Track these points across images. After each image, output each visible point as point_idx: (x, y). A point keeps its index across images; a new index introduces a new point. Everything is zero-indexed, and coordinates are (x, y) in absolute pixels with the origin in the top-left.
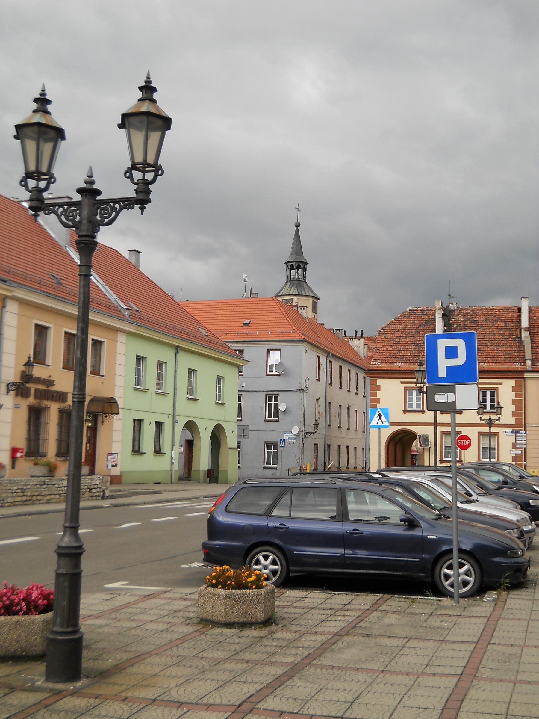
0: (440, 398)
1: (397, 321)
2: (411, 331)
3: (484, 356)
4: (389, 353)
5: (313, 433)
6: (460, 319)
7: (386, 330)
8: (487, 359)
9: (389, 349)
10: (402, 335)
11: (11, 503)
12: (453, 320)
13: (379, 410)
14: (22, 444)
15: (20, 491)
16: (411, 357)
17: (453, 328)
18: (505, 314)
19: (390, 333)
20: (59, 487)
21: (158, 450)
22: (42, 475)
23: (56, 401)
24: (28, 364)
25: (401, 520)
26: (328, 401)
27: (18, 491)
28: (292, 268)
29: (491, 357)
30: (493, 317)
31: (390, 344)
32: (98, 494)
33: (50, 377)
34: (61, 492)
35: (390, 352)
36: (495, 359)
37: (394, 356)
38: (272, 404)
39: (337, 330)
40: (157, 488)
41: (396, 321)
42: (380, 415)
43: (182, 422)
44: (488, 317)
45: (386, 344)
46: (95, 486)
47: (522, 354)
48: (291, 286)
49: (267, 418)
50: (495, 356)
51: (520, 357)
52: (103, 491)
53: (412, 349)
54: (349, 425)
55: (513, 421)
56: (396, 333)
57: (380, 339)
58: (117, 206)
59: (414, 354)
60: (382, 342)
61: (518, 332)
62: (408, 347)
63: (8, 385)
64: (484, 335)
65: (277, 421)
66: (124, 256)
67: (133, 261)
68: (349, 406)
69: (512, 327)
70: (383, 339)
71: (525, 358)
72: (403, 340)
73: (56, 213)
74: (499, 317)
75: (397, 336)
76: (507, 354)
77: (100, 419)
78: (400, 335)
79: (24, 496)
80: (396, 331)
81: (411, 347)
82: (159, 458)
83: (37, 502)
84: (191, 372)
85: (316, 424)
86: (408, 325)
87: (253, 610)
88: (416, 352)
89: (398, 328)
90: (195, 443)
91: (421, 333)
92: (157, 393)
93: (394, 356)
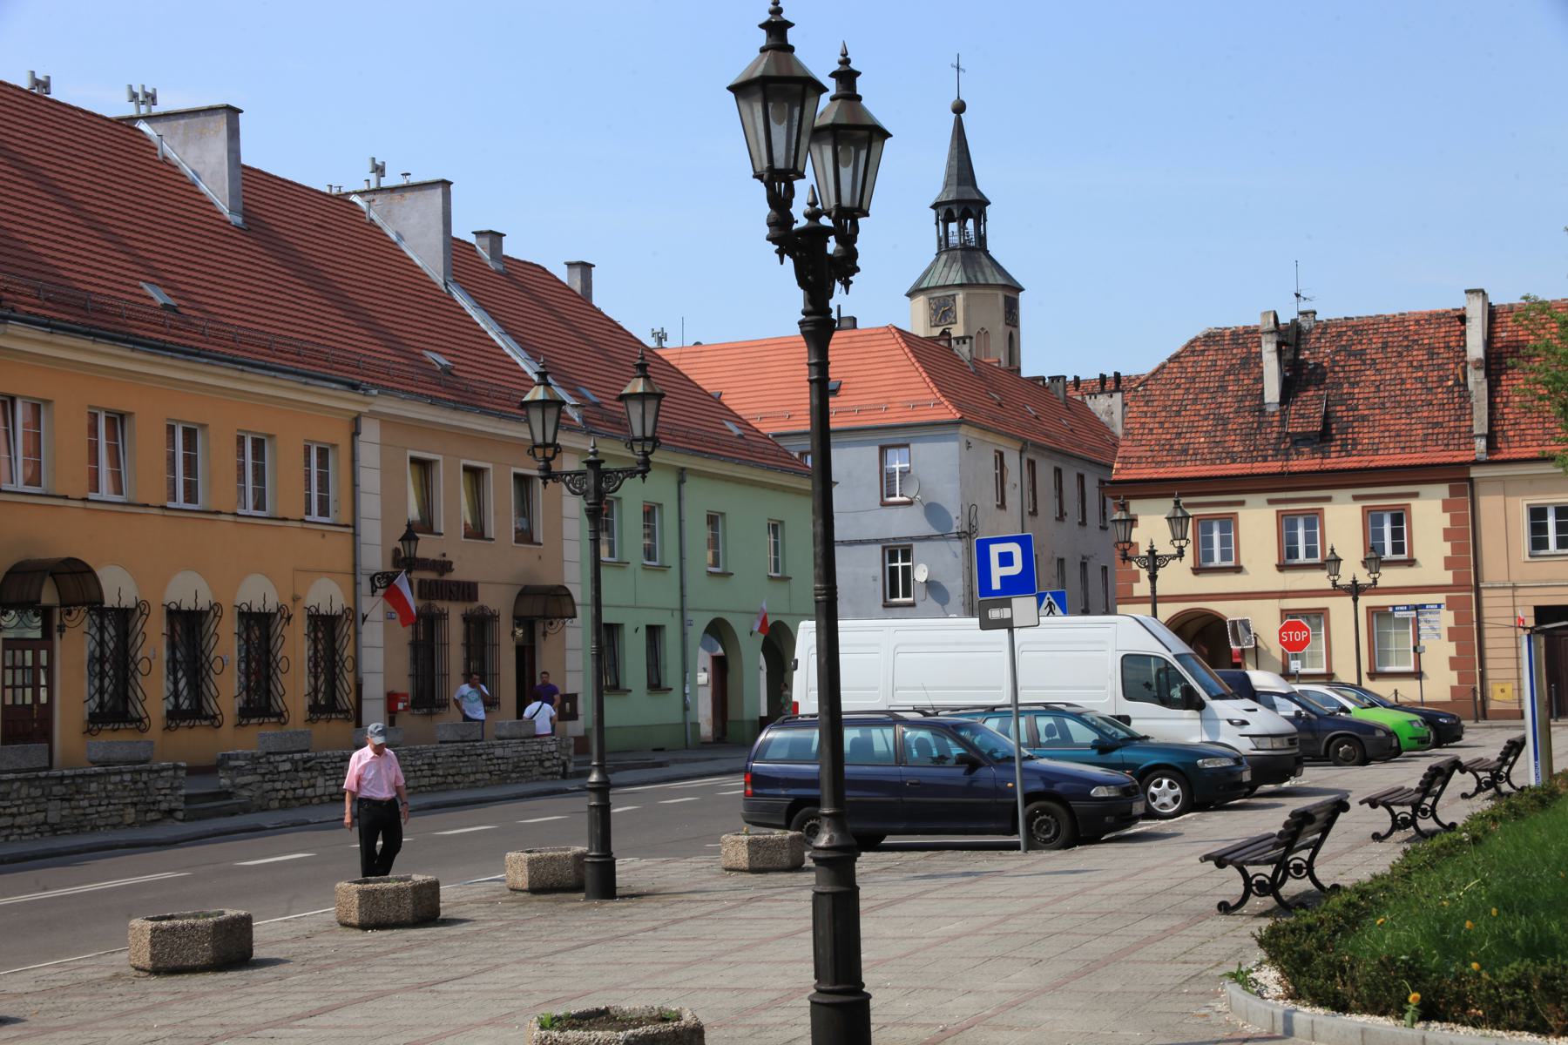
0: (994, 614)
1: (1176, 365)
2: (1207, 385)
3: (1376, 434)
4: (1156, 440)
6: (1322, 350)
7: (1149, 387)
8: (1382, 440)
9: (1155, 431)
10: (1186, 397)
11: (414, 788)
12: (1307, 352)
13: (1048, 595)
14: (404, 685)
15: (426, 767)
16: (1205, 445)
17: (1305, 371)
18: (1432, 331)
19: (1158, 393)
20: (489, 760)
21: (655, 682)
22: (459, 739)
23: (457, 600)
24: (410, 536)
27: (423, 768)
28: (948, 218)
29: (1393, 434)
30: (1401, 339)
31: (1157, 420)
32: (554, 769)
33: (444, 555)
34: (492, 767)
35: (1158, 437)
36: (1403, 439)
37: (1167, 447)
38: (897, 567)
39: (1052, 379)
40: (659, 757)
41: (1171, 365)
42: (1050, 604)
43: (700, 622)
44: (1390, 339)
45: (1148, 420)
46: (550, 756)
47: (1468, 423)
48: (948, 264)
50: (1402, 433)
51: (1463, 429)
52: (564, 765)
53: (1210, 428)
55: (1447, 578)
56: (1173, 392)
57: (1135, 409)
58: (620, 475)
59: (1212, 440)
60: (1139, 415)
62: (1201, 423)
63: (372, 579)
64: (1378, 383)
65: (912, 605)
66: (559, 277)
67: (577, 287)
68: (1084, 558)
69: (1445, 361)
70: (1141, 409)
71: (1471, 431)
72: (1188, 407)
73: (564, 481)
74: (1416, 337)
75: (1174, 400)
76: (1430, 425)
77: (539, 628)
78: (1181, 397)
79: (433, 775)
80: (1174, 386)
81: (1206, 423)
82: (659, 700)
83: (456, 787)
84: (713, 520)
86: (1200, 372)
87: (779, 856)
88: (1218, 434)
89: (1178, 381)
90: (731, 663)
91: (1230, 388)
92: (645, 567)
93: (1167, 447)
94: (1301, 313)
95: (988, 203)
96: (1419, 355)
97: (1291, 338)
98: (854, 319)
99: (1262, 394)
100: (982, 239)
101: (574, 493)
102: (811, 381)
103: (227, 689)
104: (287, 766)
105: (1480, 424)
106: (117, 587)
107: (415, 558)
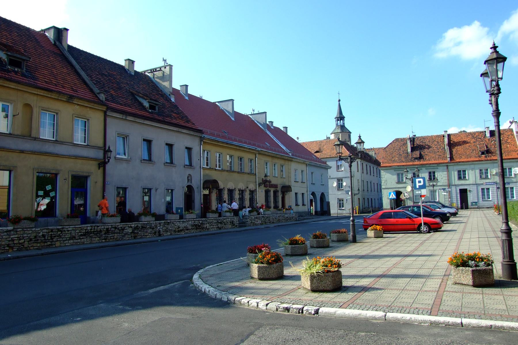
5: (358, 194)
21: (296, 204)
25: (493, 111)
26: (362, 180)
28: (338, 120)
38: (340, 183)
49: (414, 201)
54: (371, 189)
61: (443, 146)
67: (285, 132)
73: (344, 160)
85: (359, 190)
94: (413, 135)
95: (345, 117)
96: (436, 143)
97: (413, 140)
98: (329, 137)
99: (407, 150)
100: (344, 124)
101: (346, 162)
102: (495, 122)
103: (300, 202)
104: (254, 218)
105: (448, 156)
106: (221, 185)
107: (267, 180)
